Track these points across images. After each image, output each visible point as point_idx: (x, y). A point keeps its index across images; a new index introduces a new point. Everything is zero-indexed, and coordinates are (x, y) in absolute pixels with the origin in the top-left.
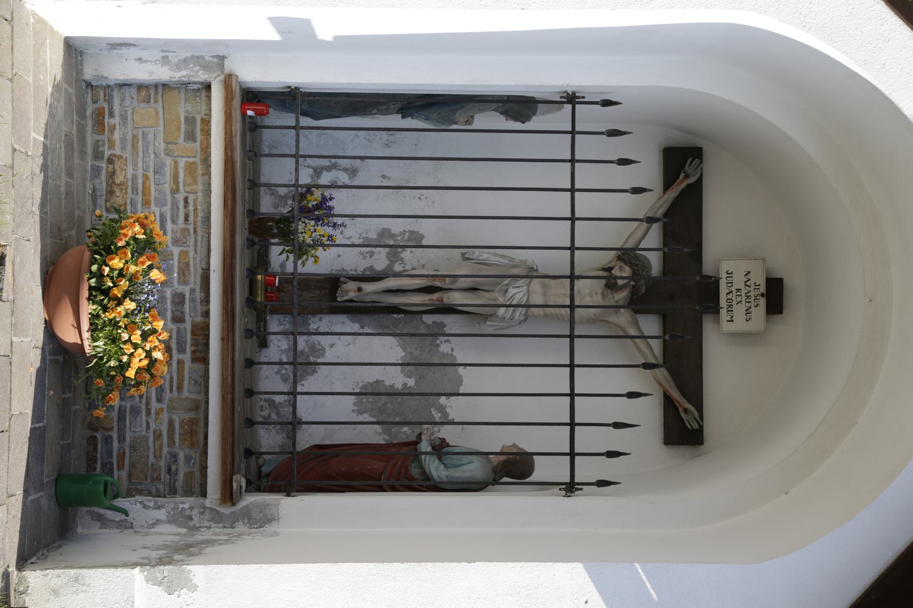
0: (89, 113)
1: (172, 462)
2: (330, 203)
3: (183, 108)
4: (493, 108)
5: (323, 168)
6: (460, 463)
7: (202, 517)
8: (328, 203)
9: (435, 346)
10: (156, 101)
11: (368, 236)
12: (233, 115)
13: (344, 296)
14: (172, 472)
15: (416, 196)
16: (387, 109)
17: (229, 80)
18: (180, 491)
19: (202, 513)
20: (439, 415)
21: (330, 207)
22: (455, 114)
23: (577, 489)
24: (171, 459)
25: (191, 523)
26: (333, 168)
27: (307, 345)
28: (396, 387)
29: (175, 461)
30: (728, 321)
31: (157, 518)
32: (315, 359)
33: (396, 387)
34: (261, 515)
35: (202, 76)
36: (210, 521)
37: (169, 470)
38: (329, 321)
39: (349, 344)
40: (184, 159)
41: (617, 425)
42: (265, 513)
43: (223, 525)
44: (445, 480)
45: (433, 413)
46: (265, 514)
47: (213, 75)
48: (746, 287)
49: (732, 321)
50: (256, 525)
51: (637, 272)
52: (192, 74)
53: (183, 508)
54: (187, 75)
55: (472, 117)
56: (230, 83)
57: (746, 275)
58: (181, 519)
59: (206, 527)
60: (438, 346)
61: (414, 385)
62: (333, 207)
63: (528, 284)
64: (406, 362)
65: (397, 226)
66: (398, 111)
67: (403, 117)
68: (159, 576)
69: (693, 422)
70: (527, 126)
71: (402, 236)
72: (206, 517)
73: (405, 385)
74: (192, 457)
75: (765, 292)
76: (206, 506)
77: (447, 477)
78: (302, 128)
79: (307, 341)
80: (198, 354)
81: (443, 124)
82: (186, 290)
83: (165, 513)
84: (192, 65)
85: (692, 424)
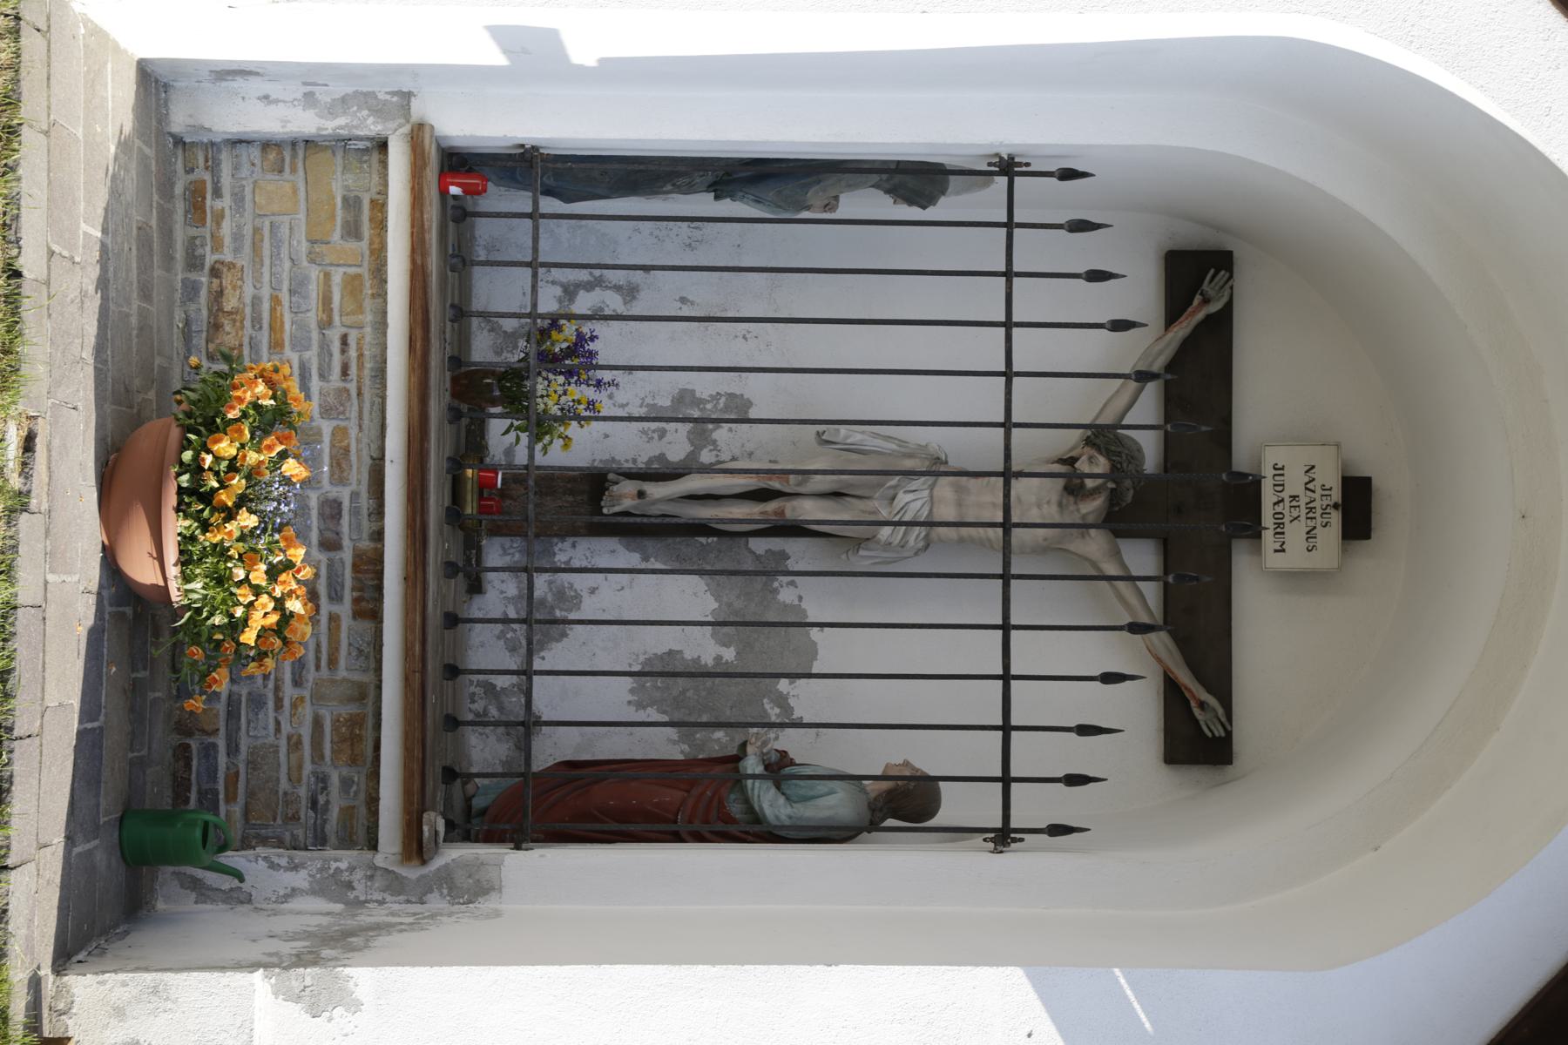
0: (179, 189)
1: (319, 788)
2: (591, 346)
3: (339, 181)
4: (872, 183)
5: (579, 286)
6: (811, 793)
7: (369, 883)
8: (588, 345)
9: (771, 592)
10: (294, 170)
11: (656, 402)
12: (426, 193)
13: (614, 506)
14: (319, 806)
15: (738, 334)
16: (690, 183)
17: (418, 134)
18: (333, 839)
19: (371, 878)
20: (777, 710)
21: (590, 352)
22: (807, 193)
23: (1015, 840)
24: (317, 785)
25: (351, 895)
26: (596, 286)
27: (551, 589)
28: (703, 663)
29: (325, 788)
30: (1276, 551)
31: (293, 885)
32: (563, 613)
33: (703, 663)
34: (471, 881)
35: (372, 127)
36: (384, 891)
37: (314, 804)
38: (589, 549)
39: (623, 588)
40: (341, 270)
41: (1084, 730)
42: (477, 877)
43: (406, 898)
44: (787, 822)
45: (767, 707)
46: (478, 880)
47: (392, 125)
48: (1307, 492)
49: (1283, 551)
50: (463, 897)
51: (1119, 466)
52: (355, 123)
53: (337, 868)
54: (347, 125)
55: (836, 198)
56: (420, 139)
57: (1307, 471)
58: (333, 888)
59: (377, 901)
60: (776, 591)
61: (733, 659)
62: (597, 353)
63: (930, 486)
64: (721, 620)
65: (705, 385)
66: (709, 186)
67: (717, 198)
68: (296, 985)
69: (1214, 725)
70: (931, 214)
71: (715, 402)
72: (377, 885)
73: (718, 658)
74: (353, 781)
75: (1340, 502)
76: (377, 865)
77: (790, 817)
78: (543, 216)
79: (550, 583)
80: (364, 604)
81: (786, 210)
82: (344, 494)
83: (307, 876)
84: (355, 108)
85: (1212, 727)
